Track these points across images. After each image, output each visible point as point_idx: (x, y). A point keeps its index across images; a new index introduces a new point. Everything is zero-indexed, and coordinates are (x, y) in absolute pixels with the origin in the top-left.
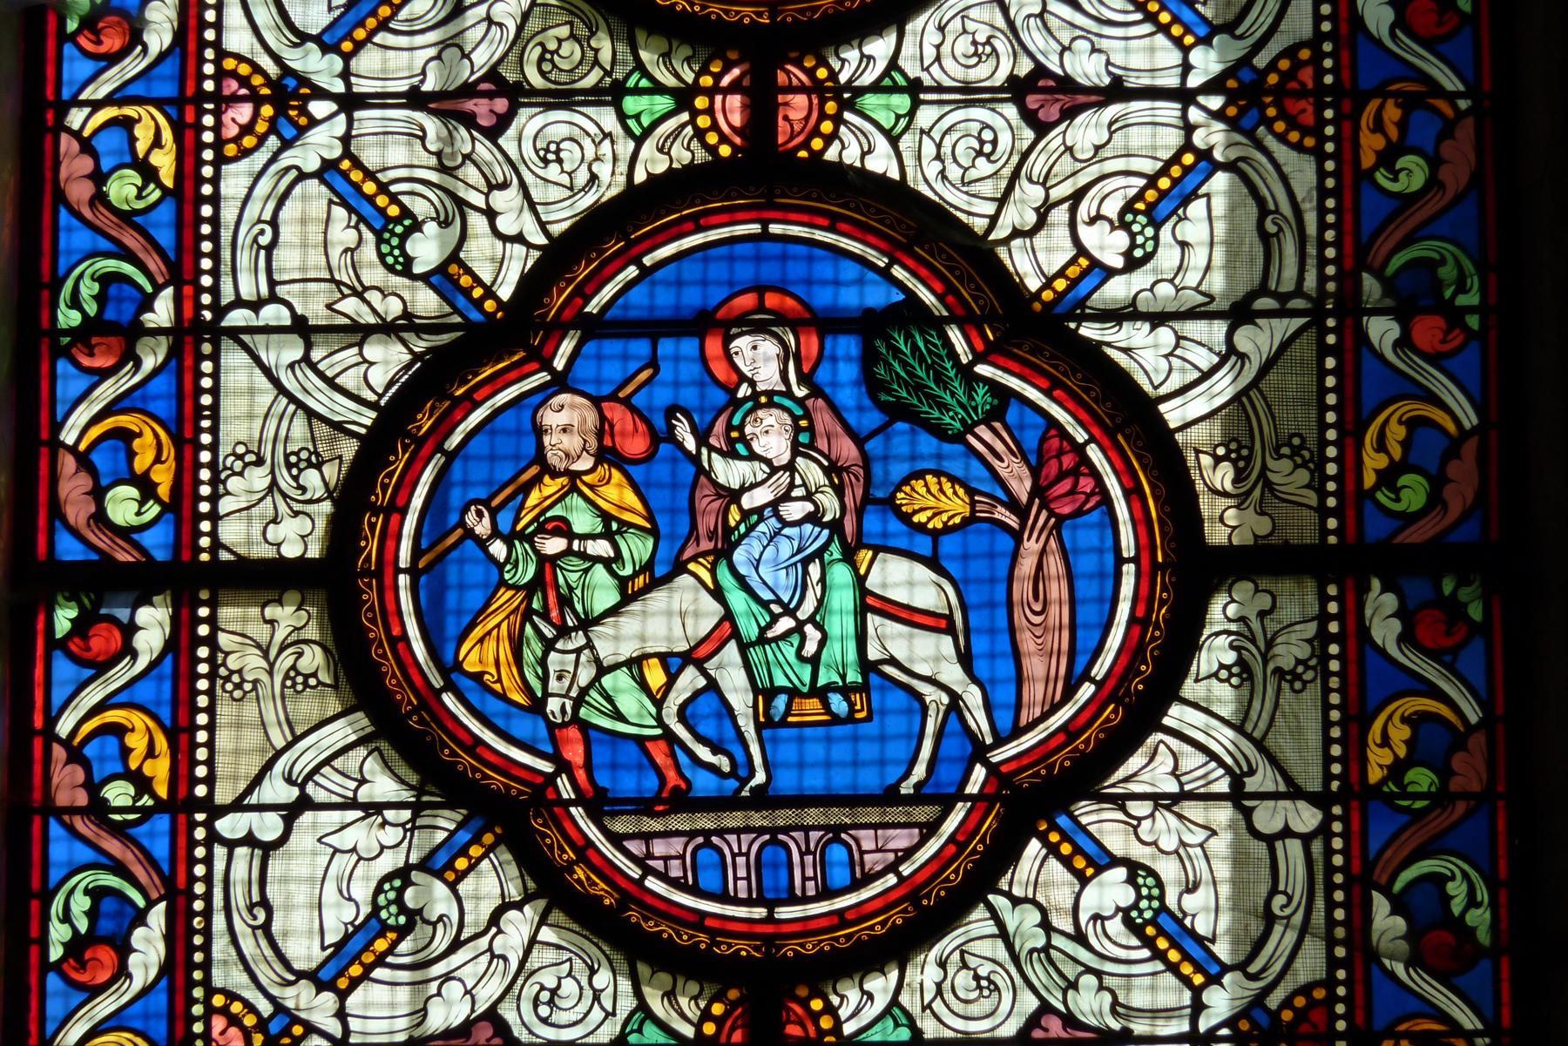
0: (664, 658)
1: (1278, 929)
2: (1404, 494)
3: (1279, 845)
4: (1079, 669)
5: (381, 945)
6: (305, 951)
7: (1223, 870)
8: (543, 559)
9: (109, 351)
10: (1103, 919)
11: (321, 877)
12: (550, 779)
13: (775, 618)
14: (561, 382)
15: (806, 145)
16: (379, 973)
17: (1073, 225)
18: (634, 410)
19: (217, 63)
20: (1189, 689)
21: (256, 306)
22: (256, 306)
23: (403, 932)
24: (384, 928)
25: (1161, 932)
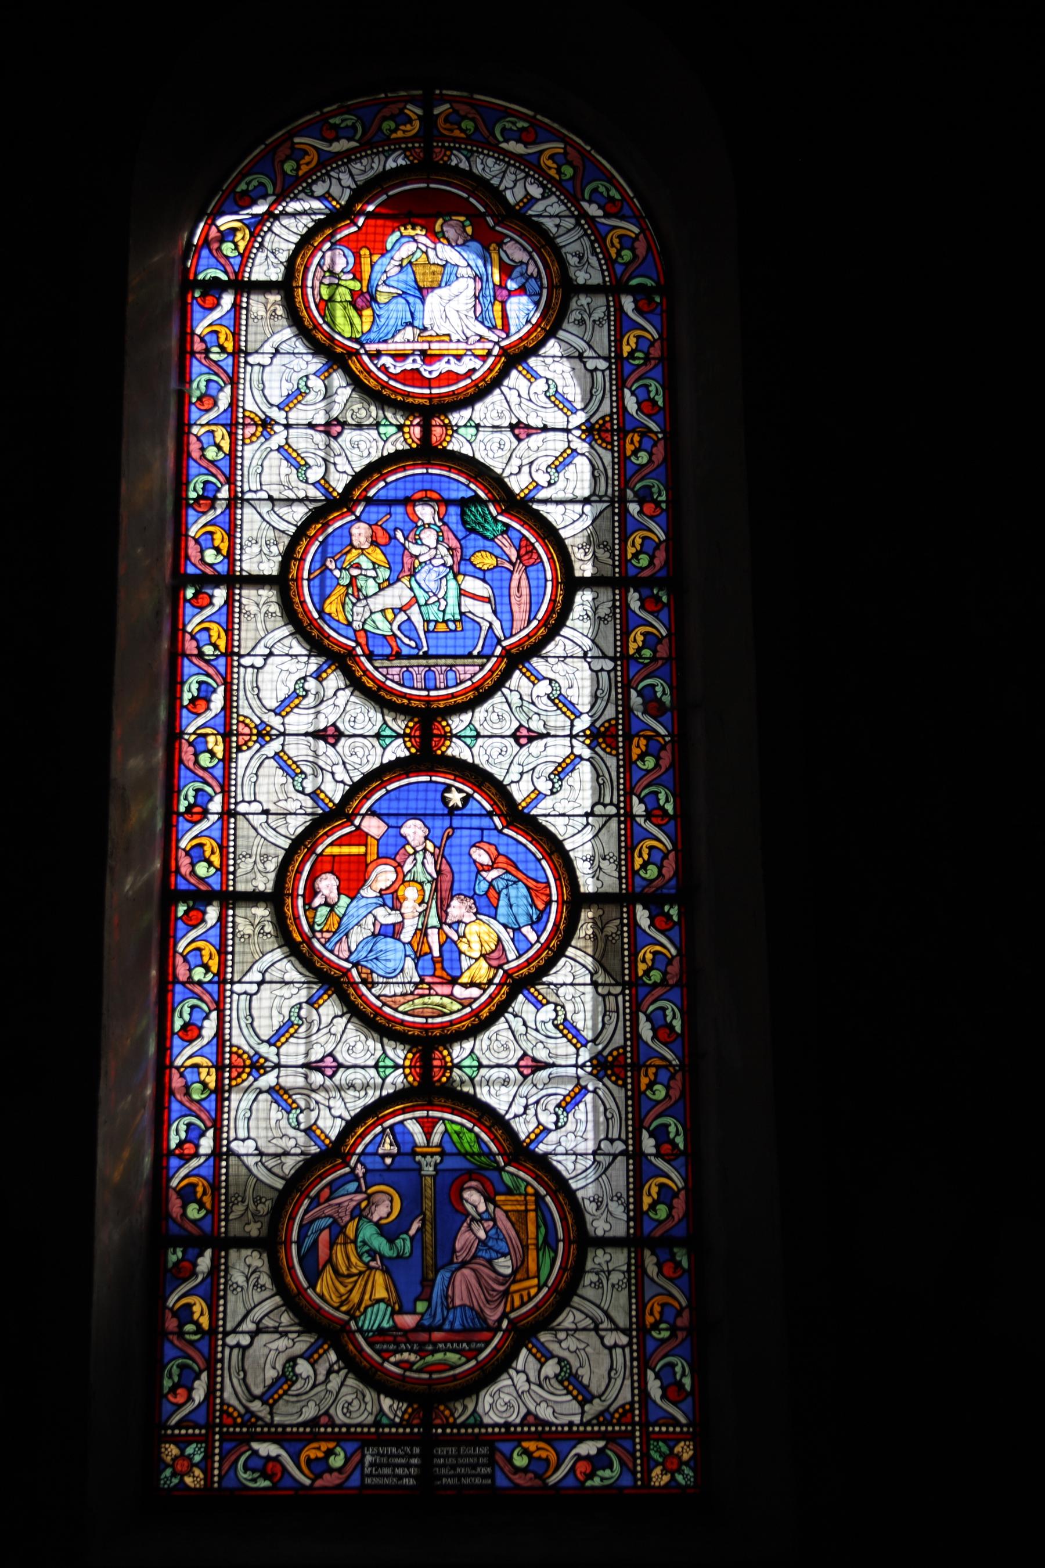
5: (297, 701)
6: (266, 1033)
14: (358, 519)
17: (536, 1115)
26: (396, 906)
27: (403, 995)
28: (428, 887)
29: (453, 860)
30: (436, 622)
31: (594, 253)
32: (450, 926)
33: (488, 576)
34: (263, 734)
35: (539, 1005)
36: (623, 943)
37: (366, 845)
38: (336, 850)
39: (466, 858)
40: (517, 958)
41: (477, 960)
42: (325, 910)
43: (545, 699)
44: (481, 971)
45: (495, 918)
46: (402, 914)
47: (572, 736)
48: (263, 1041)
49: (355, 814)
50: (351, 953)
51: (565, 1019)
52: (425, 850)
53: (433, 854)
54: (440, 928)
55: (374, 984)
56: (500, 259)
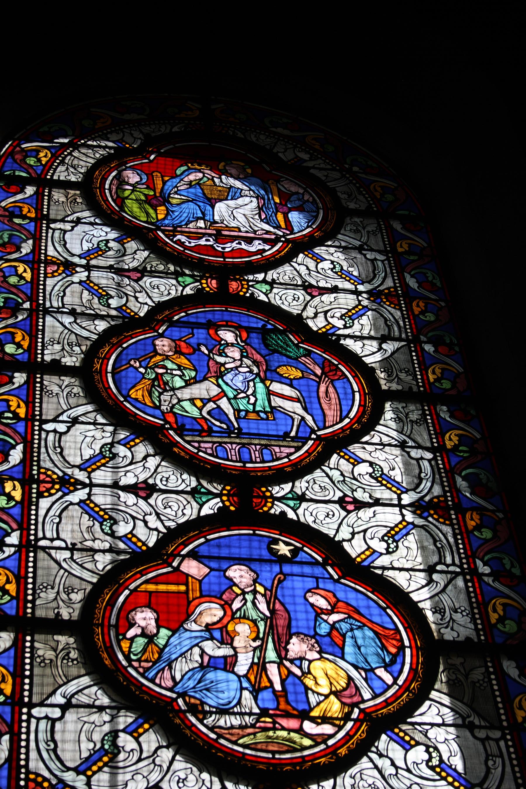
0: (201, 400)
1: (424, 482)
2: (507, 626)
3: (55, 536)
4: (344, 414)
5: (103, 461)
6: (72, 759)
7: (401, 465)
8: (157, 374)
9: (7, 314)
10: (417, 764)
11: (78, 734)
12: (164, 425)
13: (239, 394)
14: (161, 336)
15: (262, 509)
16: (102, 468)
18: (187, 343)
19: (38, 470)
20: (89, 588)
21: (52, 540)
22: (52, 540)
23: (111, 459)
24: (104, 457)
25: (383, 479)
26: (227, 639)
27: (241, 727)
28: (261, 626)
29: (287, 600)
30: (247, 412)
31: (360, 193)
32: (292, 661)
33: (295, 382)
34: (68, 484)
35: (407, 746)
36: (494, 691)
37: (187, 584)
38: (151, 587)
39: (302, 600)
40: (373, 698)
41: (327, 697)
42: (141, 642)
43: (367, 477)
44: (334, 707)
45: (343, 658)
46: (234, 649)
47: (401, 507)
48: (69, 769)
49: (174, 555)
50: (176, 683)
51: (441, 761)
52: (255, 592)
53: (264, 595)
54: (280, 665)
55: (206, 714)
56: (279, 189)
